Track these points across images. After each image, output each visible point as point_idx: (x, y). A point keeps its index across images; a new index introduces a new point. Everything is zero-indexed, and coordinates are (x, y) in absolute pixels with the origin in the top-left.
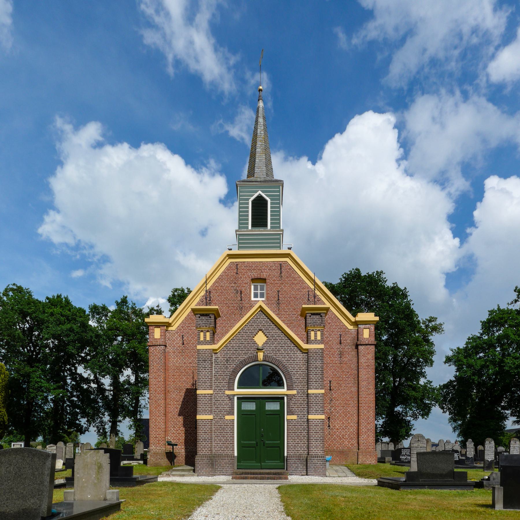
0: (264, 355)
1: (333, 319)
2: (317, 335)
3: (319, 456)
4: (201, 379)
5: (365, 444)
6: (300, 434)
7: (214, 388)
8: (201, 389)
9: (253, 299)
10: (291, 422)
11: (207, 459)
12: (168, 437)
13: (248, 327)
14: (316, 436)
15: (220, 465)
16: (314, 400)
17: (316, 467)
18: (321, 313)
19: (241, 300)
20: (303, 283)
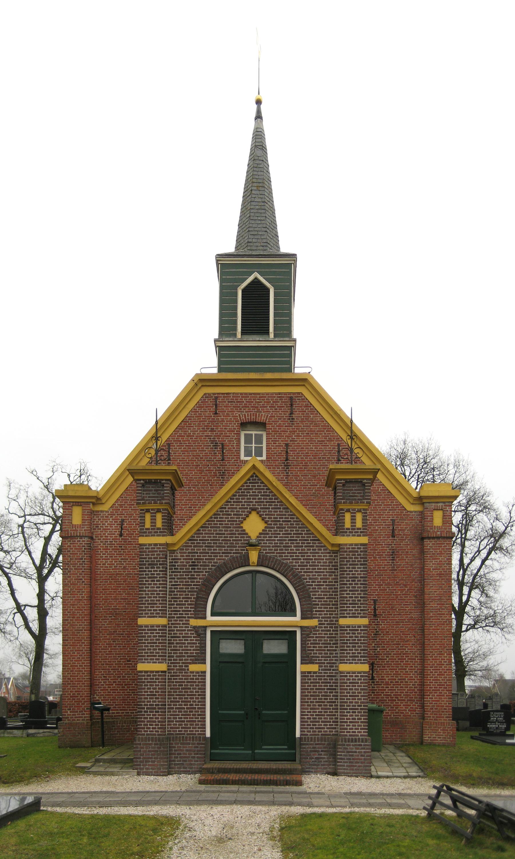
0: (259, 556)
1: (381, 493)
2: (355, 519)
3: (359, 739)
4: (145, 598)
5: (435, 709)
6: (325, 699)
7: (169, 614)
8: (145, 617)
9: (243, 457)
10: (308, 676)
11: (155, 744)
12: (95, 696)
13: (231, 505)
14: (352, 702)
15: (178, 754)
16: (350, 637)
17: (353, 759)
18: (364, 479)
19: (222, 460)
20: (329, 431)
